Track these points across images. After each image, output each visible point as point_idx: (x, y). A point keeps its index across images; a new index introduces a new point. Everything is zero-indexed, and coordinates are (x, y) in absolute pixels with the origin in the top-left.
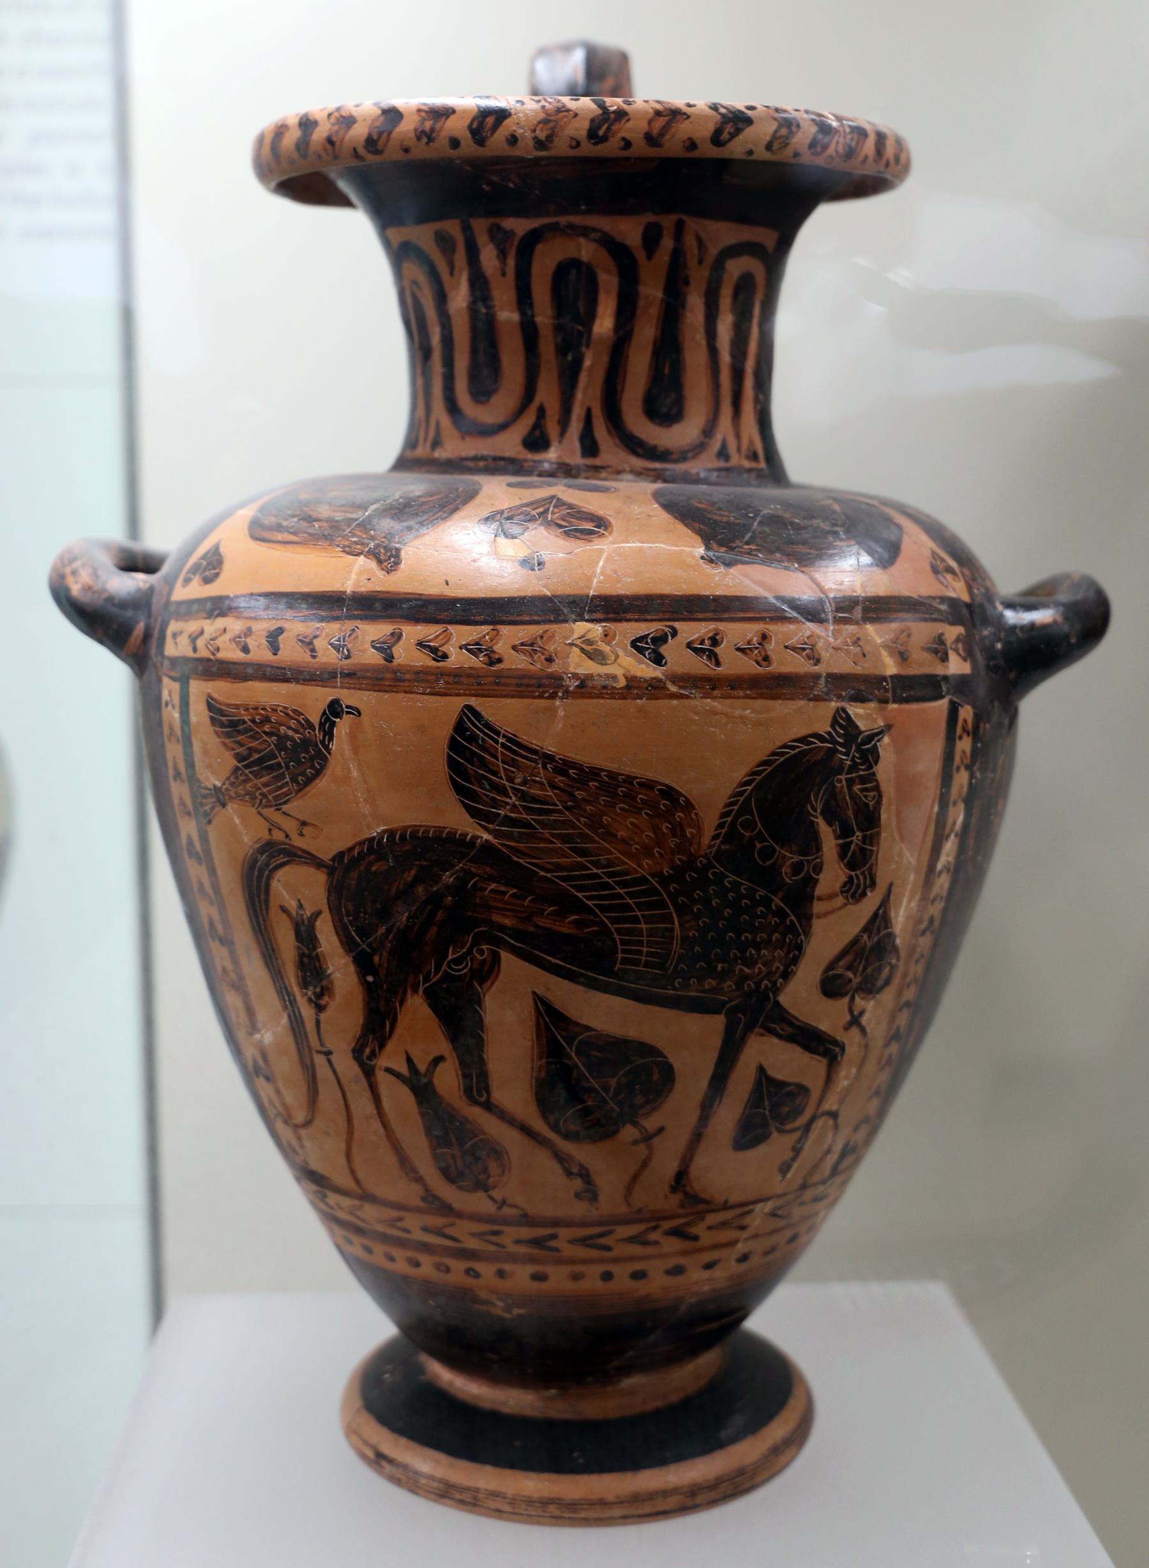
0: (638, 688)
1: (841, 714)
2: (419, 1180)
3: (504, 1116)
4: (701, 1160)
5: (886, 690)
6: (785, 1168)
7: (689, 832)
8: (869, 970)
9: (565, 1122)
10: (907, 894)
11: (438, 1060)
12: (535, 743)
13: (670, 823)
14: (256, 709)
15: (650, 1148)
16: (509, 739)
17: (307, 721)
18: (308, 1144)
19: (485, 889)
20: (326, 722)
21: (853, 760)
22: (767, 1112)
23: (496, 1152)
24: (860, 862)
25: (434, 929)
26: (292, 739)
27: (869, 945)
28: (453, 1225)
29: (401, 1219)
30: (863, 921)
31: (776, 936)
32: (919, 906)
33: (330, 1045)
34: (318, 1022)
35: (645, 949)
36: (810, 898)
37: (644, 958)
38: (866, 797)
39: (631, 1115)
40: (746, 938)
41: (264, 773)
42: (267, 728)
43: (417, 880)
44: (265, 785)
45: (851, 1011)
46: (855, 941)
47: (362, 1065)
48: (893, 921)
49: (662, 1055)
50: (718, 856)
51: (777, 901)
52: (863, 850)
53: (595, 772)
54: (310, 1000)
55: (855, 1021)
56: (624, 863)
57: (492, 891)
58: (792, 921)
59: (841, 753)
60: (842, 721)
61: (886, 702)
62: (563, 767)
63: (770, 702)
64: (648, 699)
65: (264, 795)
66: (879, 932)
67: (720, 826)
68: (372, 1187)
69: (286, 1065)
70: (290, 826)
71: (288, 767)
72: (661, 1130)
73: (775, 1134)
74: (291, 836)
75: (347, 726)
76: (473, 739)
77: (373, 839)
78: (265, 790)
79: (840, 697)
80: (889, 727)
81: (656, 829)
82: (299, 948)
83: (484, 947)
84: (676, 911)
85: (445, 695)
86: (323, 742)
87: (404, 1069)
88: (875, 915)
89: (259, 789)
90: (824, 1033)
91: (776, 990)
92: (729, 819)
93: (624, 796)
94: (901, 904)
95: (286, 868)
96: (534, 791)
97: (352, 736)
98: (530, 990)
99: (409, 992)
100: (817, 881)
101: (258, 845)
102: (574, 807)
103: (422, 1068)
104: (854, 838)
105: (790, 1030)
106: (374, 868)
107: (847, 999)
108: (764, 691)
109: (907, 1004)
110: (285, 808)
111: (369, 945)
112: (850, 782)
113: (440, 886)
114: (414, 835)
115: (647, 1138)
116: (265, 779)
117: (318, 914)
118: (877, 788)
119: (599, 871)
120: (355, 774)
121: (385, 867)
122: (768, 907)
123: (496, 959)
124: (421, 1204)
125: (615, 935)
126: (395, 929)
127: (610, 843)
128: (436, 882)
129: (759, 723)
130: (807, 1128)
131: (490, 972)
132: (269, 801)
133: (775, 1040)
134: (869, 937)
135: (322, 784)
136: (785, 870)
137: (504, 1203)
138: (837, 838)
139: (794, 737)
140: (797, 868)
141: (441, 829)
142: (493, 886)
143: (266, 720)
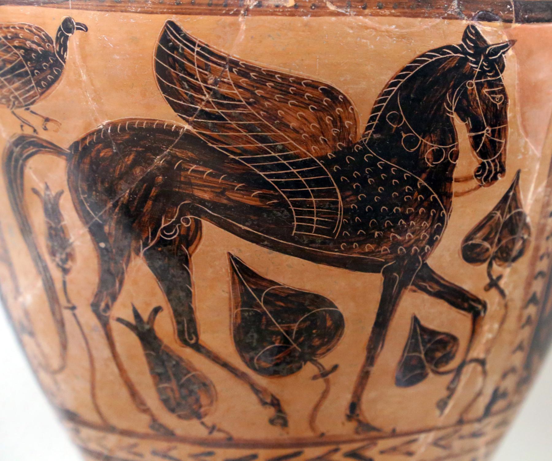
0: (303, 7)
1: (470, 29)
2: (147, 411)
3: (215, 359)
4: (368, 395)
5: (510, 12)
6: (442, 405)
7: (347, 123)
8: (504, 242)
9: (258, 360)
10: (534, 180)
11: (157, 310)
12: (223, 51)
13: (332, 116)
14: (8, 28)
15: (327, 382)
16: (203, 49)
17: (47, 36)
18: (63, 386)
19: (188, 170)
20: (61, 36)
21: (481, 68)
22: (423, 356)
23: (205, 385)
24: (491, 154)
25: (150, 203)
26: (36, 51)
27: (502, 221)
28: (175, 448)
29: (135, 445)
30: (496, 201)
31: (421, 210)
32: (546, 191)
33: (75, 302)
34: (64, 283)
35: (315, 219)
36: (450, 180)
37: (315, 226)
38: (494, 98)
39: (311, 354)
40: (397, 210)
41: (15, 79)
42: (16, 43)
43: (135, 163)
44: (17, 89)
45: (490, 275)
46: (490, 217)
47: (99, 317)
48: (523, 202)
49: (332, 304)
50: (372, 143)
51: (421, 181)
52: (492, 142)
53: (270, 75)
54: (58, 265)
55: (494, 284)
56: (296, 148)
57: (193, 171)
58: (434, 198)
59: (471, 62)
60: (473, 37)
61: (510, 21)
62: (245, 70)
63: (411, 20)
64: (312, 16)
65: (16, 98)
66: (510, 211)
67: (372, 119)
68: (115, 421)
69: (44, 321)
70: (36, 122)
71: (33, 75)
72: (335, 368)
73: (431, 375)
74: (38, 130)
75: (77, 40)
76: (174, 48)
77: (99, 131)
78: (16, 94)
79: (469, 17)
80: (513, 42)
81: (320, 120)
82: (48, 223)
83: (189, 217)
84: (339, 188)
85: (152, 13)
86: (59, 53)
87: (131, 319)
88: (505, 198)
89: (12, 93)
90: (468, 292)
91: (425, 256)
92: (379, 113)
93: (295, 94)
94: (528, 190)
95: (36, 157)
96: (224, 90)
97: (82, 47)
98: (226, 252)
99: (133, 255)
100: (455, 165)
101: (14, 139)
102: (255, 103)
103: (145, 316)
104: (485, 132)
105: (437, 288)
106: (102, 154)
107: (485, 265)
108: (407, 10)
109: (541, 274)
110: (32, 107)
111: (100, 218)
112: (480, 86)
113: (152, 167)
114: (131, 127)
115: (324, 374)
116: (17, 84)
117: (61, 193)
118: (503, 91)
119: (276, 155)
120: (84, 77)
121: (111, 153)
122: (414, 185)
123: (198, 226)
124: (150, 431)
125: (291, 207)
126: (120, 203)
127: (284, 131)
128: (150, 165)
129: (402, 37)
130: (459, 370)
131: (194, 237)
132: (20, 102)
133: (426, 296)
134: (502, 214)
135: (59, 87)
136: (428, 155)
137: (212, 429)
138: (471, 131)
139: (432, 48)
140: (437, 154)
141: (151, 122)
142: (194, 167)
143: (16, 36)
